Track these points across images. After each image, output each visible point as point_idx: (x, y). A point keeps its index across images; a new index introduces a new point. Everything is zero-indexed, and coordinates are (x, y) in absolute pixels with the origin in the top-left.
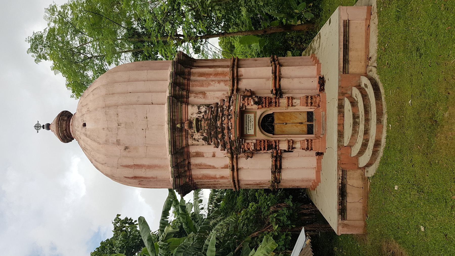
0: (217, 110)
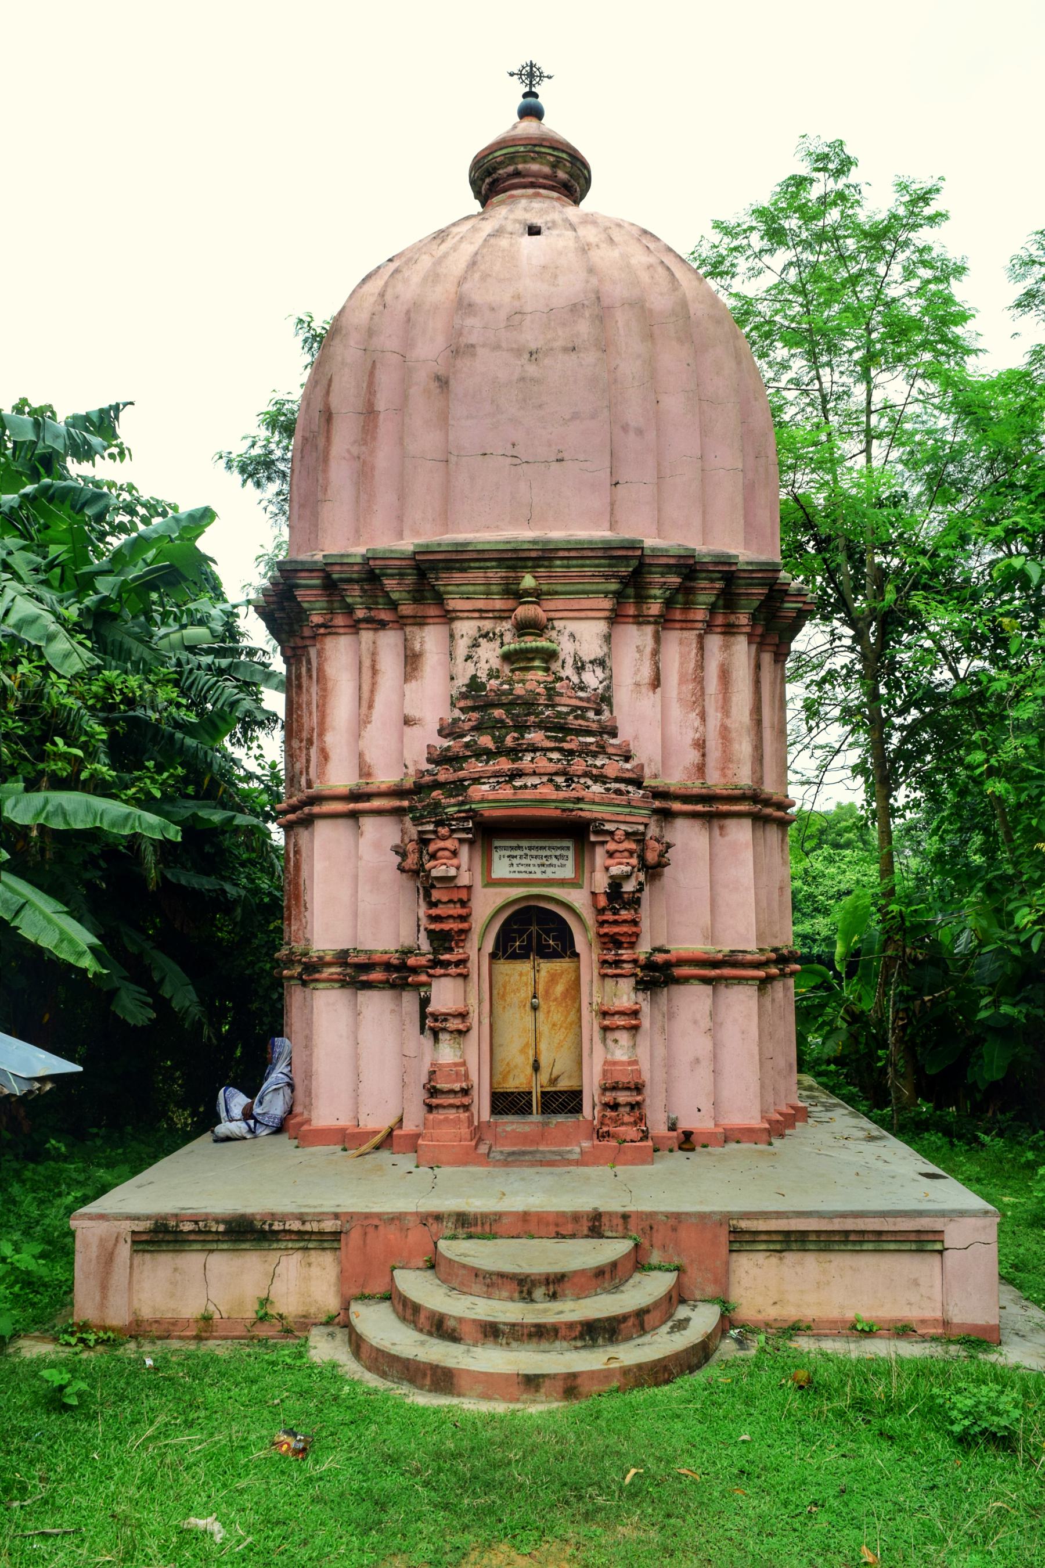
0: (589, 733)
